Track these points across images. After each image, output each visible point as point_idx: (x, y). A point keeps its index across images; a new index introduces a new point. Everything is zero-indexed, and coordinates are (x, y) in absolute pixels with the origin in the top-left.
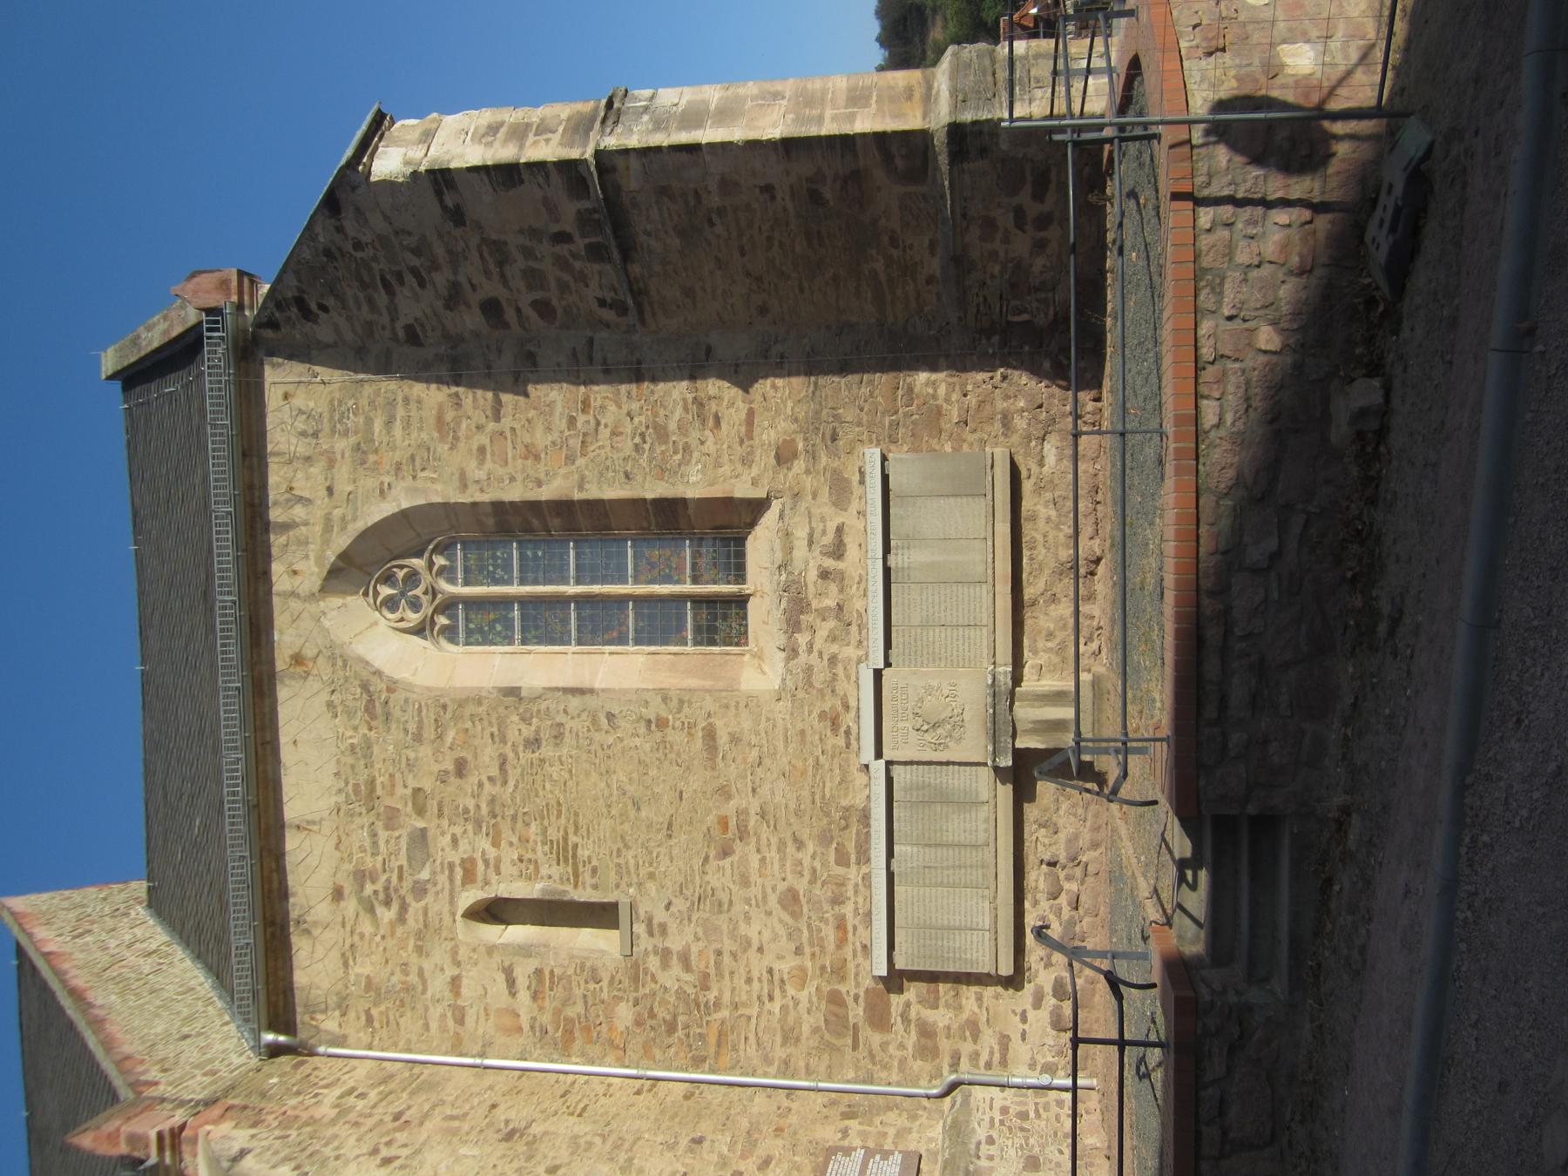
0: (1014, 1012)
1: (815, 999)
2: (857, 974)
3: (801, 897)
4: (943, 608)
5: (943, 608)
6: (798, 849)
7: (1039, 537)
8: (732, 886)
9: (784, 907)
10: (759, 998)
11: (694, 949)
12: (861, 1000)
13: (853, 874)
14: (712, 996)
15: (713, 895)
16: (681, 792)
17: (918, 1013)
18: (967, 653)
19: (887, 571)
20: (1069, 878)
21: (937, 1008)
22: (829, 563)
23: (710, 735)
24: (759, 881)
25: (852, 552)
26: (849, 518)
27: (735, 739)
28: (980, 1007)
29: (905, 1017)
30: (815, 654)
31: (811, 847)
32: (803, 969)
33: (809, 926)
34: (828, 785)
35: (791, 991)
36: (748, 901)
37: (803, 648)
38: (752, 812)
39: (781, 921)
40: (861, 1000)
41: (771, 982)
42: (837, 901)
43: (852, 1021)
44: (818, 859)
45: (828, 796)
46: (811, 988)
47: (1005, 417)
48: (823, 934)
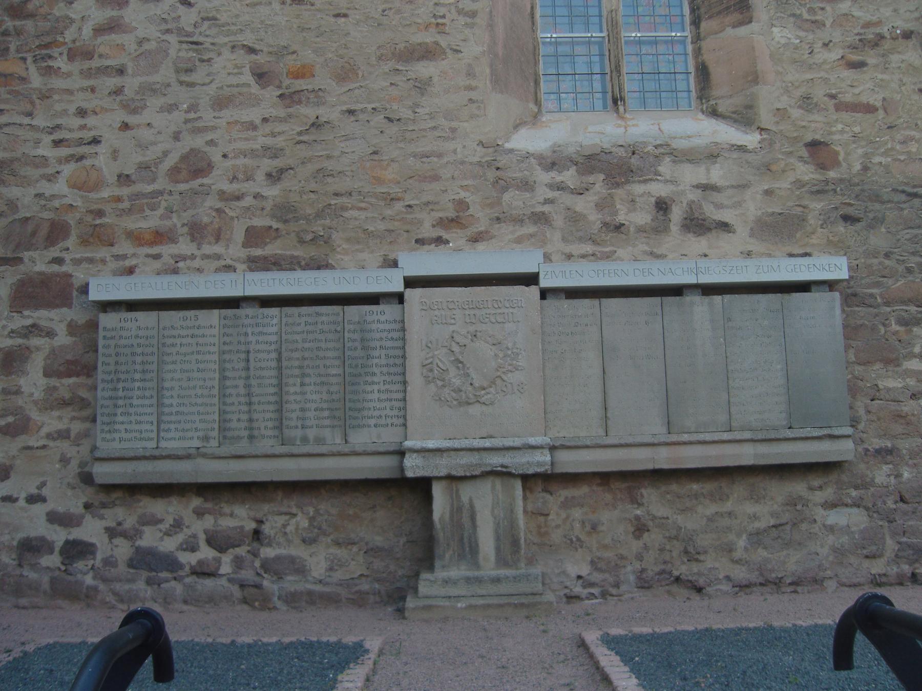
0: (43, 484)
1: (56, 203)
2: (91, 261)
3: (200, 181)
6: (269, 175)
7: (728, 506)
8: (214, 86)
9: (184, 158)
10: (58, 127)
11: (128, 40)
12: (55, 268)
13: (235, 251)
14: (61, 63)
15: (202, 61)
16: (345, 16)
19: (676, 291)
20: (238, 563)
22: (677, 214)
23: (428, 53)
24: (222, 123)
25: (698, 244)
26: (741, 238)
27: (422, 86)
28: (49, 436)
29: (34, 329)
30: (550, 194)
31: (272, 192)
32: (98, 185)
33: (161, 193)
34: (363, 215)
35: (68, 169)
36: (193, 108)
38: (321, 111)
39: (166, 154)
40: (55, 268)
41: (80, 142)
42: (196, 231)
43: (26, 255)
45: (346, 214)
46: (74, 198)
47: (890, 451)
48: (148, 212)
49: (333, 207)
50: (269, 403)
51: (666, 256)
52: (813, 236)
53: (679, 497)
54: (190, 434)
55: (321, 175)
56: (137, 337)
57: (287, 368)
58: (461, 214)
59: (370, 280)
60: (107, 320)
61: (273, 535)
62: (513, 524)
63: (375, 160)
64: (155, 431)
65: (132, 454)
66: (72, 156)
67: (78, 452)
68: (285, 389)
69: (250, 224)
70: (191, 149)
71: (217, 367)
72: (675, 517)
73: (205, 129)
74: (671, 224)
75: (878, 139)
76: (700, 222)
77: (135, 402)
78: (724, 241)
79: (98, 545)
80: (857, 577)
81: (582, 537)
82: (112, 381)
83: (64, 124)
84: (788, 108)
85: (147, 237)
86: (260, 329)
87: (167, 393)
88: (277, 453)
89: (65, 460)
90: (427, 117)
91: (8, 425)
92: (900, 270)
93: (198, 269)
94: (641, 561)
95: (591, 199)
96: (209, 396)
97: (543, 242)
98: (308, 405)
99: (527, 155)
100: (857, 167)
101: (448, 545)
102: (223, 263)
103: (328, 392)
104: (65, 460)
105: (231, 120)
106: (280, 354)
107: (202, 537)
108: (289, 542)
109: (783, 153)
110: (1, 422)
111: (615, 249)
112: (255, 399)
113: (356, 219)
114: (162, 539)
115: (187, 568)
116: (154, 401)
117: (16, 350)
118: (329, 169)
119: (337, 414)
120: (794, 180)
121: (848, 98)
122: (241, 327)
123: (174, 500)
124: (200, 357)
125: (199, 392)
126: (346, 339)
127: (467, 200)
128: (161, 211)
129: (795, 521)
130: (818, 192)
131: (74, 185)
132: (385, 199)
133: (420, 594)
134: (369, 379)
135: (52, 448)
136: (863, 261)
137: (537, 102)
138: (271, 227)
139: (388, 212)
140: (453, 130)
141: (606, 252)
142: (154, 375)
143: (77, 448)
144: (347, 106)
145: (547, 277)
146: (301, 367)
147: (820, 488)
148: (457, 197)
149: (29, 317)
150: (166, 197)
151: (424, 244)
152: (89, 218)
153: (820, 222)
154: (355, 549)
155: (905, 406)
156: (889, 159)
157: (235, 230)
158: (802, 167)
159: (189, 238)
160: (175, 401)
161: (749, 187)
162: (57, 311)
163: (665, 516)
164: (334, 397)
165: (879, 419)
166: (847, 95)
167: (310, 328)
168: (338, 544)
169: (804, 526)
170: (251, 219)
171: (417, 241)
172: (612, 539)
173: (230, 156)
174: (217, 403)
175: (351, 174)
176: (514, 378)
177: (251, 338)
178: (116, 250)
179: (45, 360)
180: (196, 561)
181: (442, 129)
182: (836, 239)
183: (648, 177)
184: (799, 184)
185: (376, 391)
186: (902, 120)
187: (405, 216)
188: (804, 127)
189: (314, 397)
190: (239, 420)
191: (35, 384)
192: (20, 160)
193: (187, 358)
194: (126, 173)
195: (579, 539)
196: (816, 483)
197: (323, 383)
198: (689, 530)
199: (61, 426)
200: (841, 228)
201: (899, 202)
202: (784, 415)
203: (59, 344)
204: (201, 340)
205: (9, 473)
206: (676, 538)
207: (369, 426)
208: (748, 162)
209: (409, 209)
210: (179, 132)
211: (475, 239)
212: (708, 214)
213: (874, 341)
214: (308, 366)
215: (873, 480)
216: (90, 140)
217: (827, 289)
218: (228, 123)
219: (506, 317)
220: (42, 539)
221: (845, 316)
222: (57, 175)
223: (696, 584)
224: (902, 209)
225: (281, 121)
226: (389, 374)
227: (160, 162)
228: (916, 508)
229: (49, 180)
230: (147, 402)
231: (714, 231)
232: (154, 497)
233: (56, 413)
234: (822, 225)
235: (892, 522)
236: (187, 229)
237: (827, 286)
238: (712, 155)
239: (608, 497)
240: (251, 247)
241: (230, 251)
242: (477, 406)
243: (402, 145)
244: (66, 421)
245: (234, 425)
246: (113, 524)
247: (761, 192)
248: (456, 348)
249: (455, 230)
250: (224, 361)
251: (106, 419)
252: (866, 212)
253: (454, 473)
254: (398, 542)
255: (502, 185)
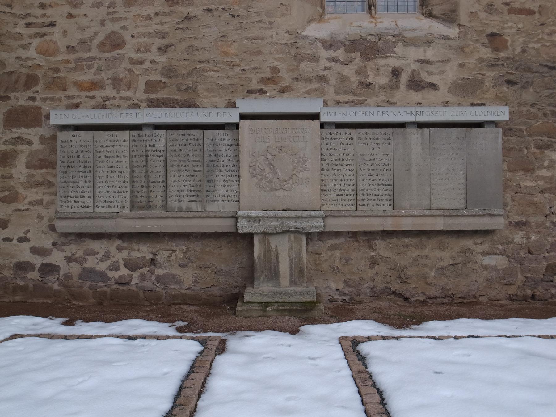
1: (30, 63)
2: (52, 99)
3: (117, 51)
4: (372, 173)
5: (372, 173)
6: (159, 49)
7: (426, 252)
9: (108, 37)
10: (28, 15)
12: (31, 103)
17: (22, 152)
18: (333, 193)
19: (402, 125)
21: (27, 167)
22: (404, 78)
24: (130, 15)
25: (416, 96)
28: (30, 203)
29: (19, 140)
30: (328, 64)
32: (54, 53)
33: (94, 58)
34: (216, 75)
35: (36, 42)
37: (333, 53)
38: (191, 9)
39: (96, 34)
40: (31, 103)
41: (43, 25)
42: (116, 83)
43: (12, 95)
44: (151, 65)
45: (207, 74)
46: (40, 60)
47: (524, 224)
48: (86, 70)
49: (198, 69)
50: (160, 187)
51: (396, 103)
52: (487, 93)
53: (397, 246)
54: (113, 204)
55: (191, 50)
56: (80, 146)
57: (170, 166)
58: (275, 75)
59: (219, 115)
60: (62, 136)
61: (162, 262)
62: (300, 260)
63: (223, 41)
64: (92, 202)
65: (78, 216)
66: (38, 33)
67: (48, 213)
68: (169, 179)
69: (148, 79)
70: (112, 32)
71: (128, 165)
72: (394, 257)
73: (120, 19)
74: (400, 84)
75: (533, 32)
76: (418, 83)
77: (80, 185)
78: (431, 95)
79: (61, 266)
80: (499, 296)
81: (340, 267)
82: (66, 172)
83: (32, 13)
84: (478, 12)
85: (86, 85)
86: (154, 143)
87: (99, 180)
88: (164, 216)
89: (40, 217)
90: (255, 14)
91: (6, 197)
92: (540, 115)
93: (118, 106)
94: (374, 282)
95: (353, 67)
96: (124, 182)
97: (323, 94)
98: (182, 188)
99: (315, 40)
100: (518, 50)
101: (262, 272)
102: (133, 102)
103: (194, 181)
104: (40, 217)
105: (136, 13)
106: (166, 158)
107: (121, 263)
108: (172, 266)
109: (472, 41)
110: (1, 195)
111: (366, 99)
112: (151, 184)
113: (212, 77)
114: (98, 263)
115: (113, 280)
116: (91, 184)
117: (9, 152)
118: (196, 46)
119: (199, 194)
120: (478, 58)
121: (517, 5)
122: (143, 141)
123: (105, 242)
124: (118, 159)
125: (118, 179)
126: (205, 150)
127: (278, 67)
128: (94, 70)
129: (465, 262)
130: (492, 65)
131: (41, 52)
132: (229, 65)
133: (245, 301)
134: (218, 173)
135: (32, 211)
136: (517, 109)
137: (322, 7)
138: (161, 81)
139: (231, 73)
140: (271, 23)
141: (361, 100)
142: (91, 169)
143: (47, 211)
144: (207, 7)
145: (325, 115)
146: (178, 166)
147: (481, 243)
148: (272, 65)
149: (15, 133)
150: (97, 61)
151: (252, 93)
152: (50, 73)
153: (492, 85)
154: (209, 271)
155: (536, 197)
156: (539, 45)
157: (139, 82)
158: (484, 50)
159: (112, 86)
160: (104, 185)
161: (450, 62)
162: (33, 129)
163: (389, 257)
164: (198, 184)
165: (519, 205)
166: (516, 3)
167: (183, 143)
168: (200, 268)
169: (470, 265)
170: (149, 76)
171: (248, 91)
172: (357, 269)
173: (135, 36)
174: (129, 186)
175: (209, 49)
176: (304, 175)
177: (148, 148)
178: (68, 93)
179: (26, 158)
180: (118, 276)
181: (264, 22)
182: (502, 95)
183: (387, 55)
184: (481, 60)
185: (222, 181)
186: (550, 20)
187: (241, 76)
188: (487, 24)
189: (186, 183)
190: (142, 196)
191: (21, 173)
192: (5, 35)
193: (111, 159)
194: (72, 45)
195: (338, 268)
196: (479, 241)
197: (191, 176)
198: (402, 265)
199: (38, 197)
200: (505, 88)
201: (542, 73)
202: (463, 201)
203: (35, 149)
204: (119, 149)
205: (7, 224)
206: (394, 269)
207: (218, 201)
208: (450, 46)
209: (244, 72)
210: (104, 21)
211: (283, 91)
212: (423, 79)
213: (520, 158)
214: (182, 165)
215: (513, 240)
216: (49, 24)
217: (495, 126)
218: (134, 15)
219: (300, 139)
220: (28, 263)
221: (503, 142)
222: (29, 45)
223: (405, 296)
224: (545, 77)
225: (166, 15)
226: (230, 171)
227: (93, 39)
228: (537, 257)
229: (25, 49)
230: (87, 185)
231: (426, 89)
232: (93, 239)
233: (34, 190)
234: (494, 86)
235: (522, 265)
236: (111, 81)
237: (494, 124)
238: (428, 42)
239: (356, 244)
240: (149, 93)
241: (137, 95)
242: (281, 191)
243: (239, 32)
244: (40, 194)
245: (139, 199)
246: (70, 255)
247: (457, 65)
248: (270, 157)
249: (271, 85)
250: (133, 161)
251: (62, 195)
252: (521, 78)
253: (267, 231)
254: (234, 267)
255: (299, 58)
